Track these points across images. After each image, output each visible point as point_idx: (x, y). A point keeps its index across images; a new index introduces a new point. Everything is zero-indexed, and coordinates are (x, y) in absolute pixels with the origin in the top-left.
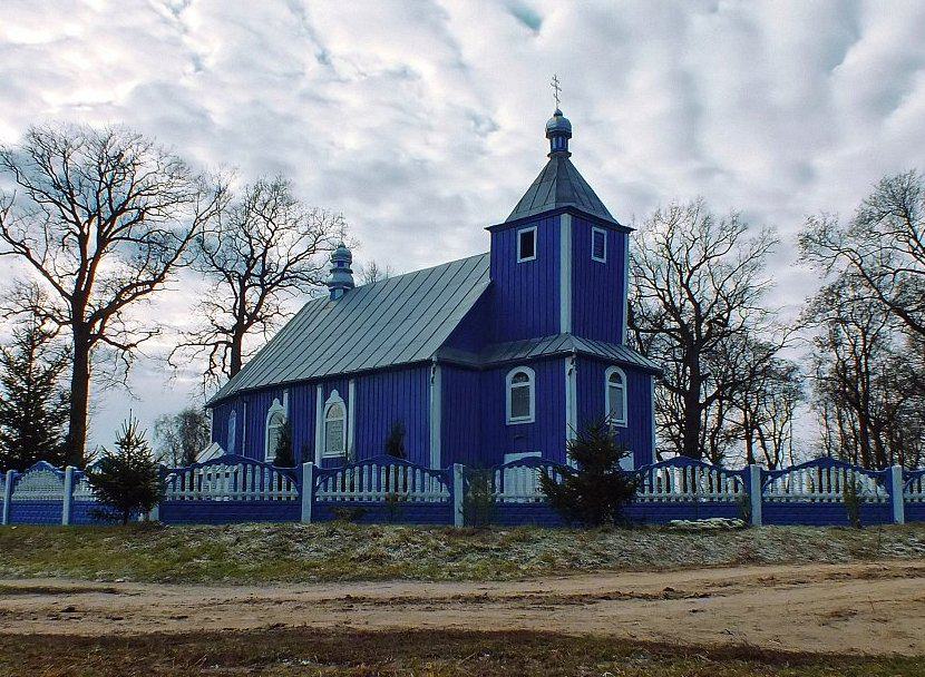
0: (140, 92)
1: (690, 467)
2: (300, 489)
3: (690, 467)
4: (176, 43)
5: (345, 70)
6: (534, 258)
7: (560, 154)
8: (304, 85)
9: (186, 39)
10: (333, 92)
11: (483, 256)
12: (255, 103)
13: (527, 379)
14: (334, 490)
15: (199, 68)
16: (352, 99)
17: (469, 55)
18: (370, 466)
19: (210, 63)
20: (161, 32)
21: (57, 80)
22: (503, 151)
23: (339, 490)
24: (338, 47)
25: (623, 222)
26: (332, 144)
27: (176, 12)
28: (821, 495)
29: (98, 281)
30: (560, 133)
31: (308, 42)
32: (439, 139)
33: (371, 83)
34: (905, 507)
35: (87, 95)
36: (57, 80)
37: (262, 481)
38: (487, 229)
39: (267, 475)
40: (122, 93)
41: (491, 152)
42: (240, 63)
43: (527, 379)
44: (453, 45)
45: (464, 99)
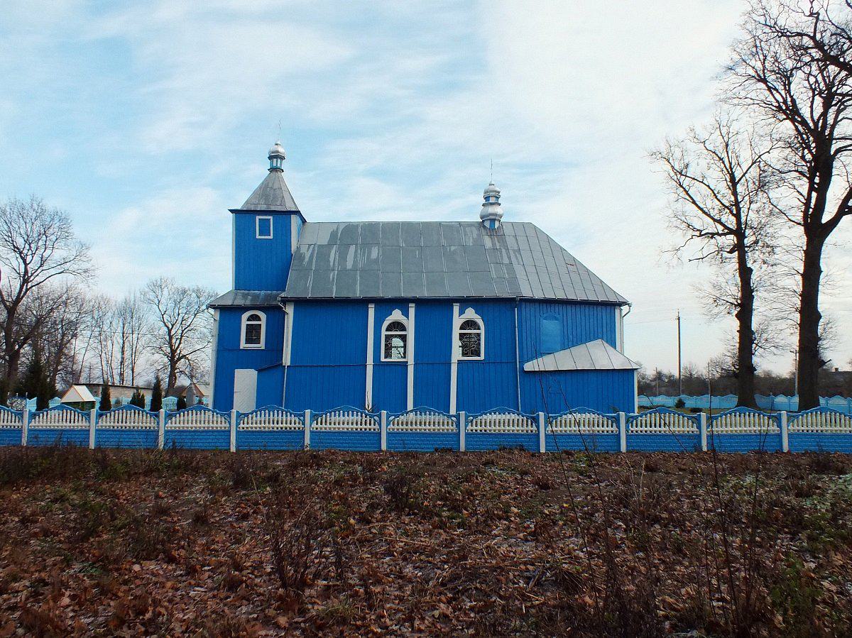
1: (133, 411)
6: (258, 237)
11: (514, 280)
13: (260, 320)
14: (565, 427)
18: (261, 412)
23: (13, 423)
38: (232, 211)
39: (77, 415)
43: (260, 320)
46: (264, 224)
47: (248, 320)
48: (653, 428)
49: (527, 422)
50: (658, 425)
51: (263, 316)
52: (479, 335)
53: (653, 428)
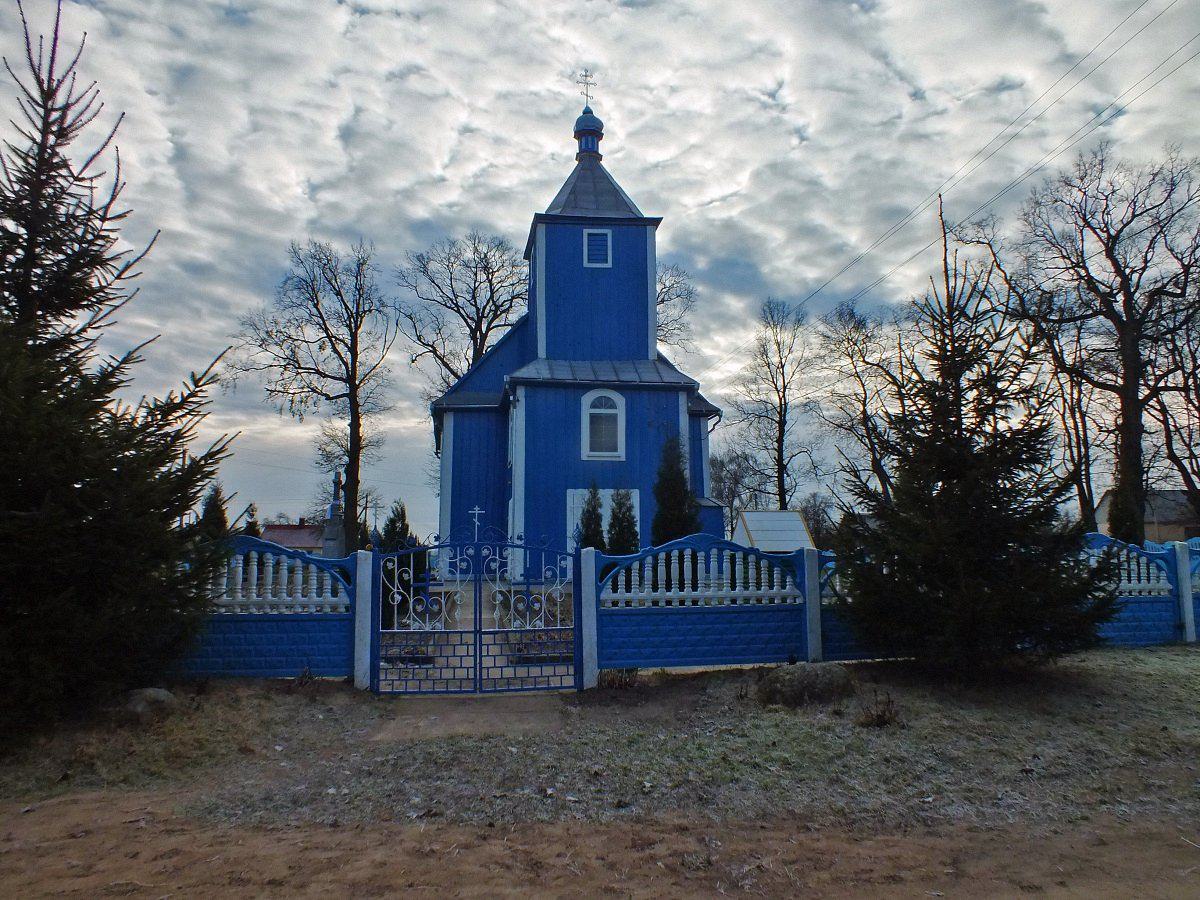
0: (757, 175)
2: (352, 594)
3: (714, 551)
4: (777, 122)
5: (941, 101)
7: (589, 155)
8: (902, 127)
9: (786, 117)
10: (933, 125)
12: (858, 158)
13: (613, 406)
15: (803, 139)
16: (954, 126)
17: (1075, 43)
19: (811, 131)
20: (763, 118)
21: (692, 185)
22: (1137, 133)
23: (1134, 582)
24: (928, 80)
25: (647, 213)
26: (941, 176)
27: (772, 95)
28: (746, 593)
29: (552, 372)
30: (589, 131)
31: (898, 83)
32: (1056, 142)
33: (969, 105)
34: (822, 611)
35: (714, 192)
36: (692, 185)
37: (746, 578)
40: (743, 180)
41: (1121, 140)
42: (839, 124)
43: (613, 406)
44: (1054, 36)
45: (1078, 91)
46: (597, 242)
47: (594, 406)
48: (674, 593)
49: (771, 575)
50: (688, 582)
51: (619, 400)
52: (614, 418)
53: (674, 593)
